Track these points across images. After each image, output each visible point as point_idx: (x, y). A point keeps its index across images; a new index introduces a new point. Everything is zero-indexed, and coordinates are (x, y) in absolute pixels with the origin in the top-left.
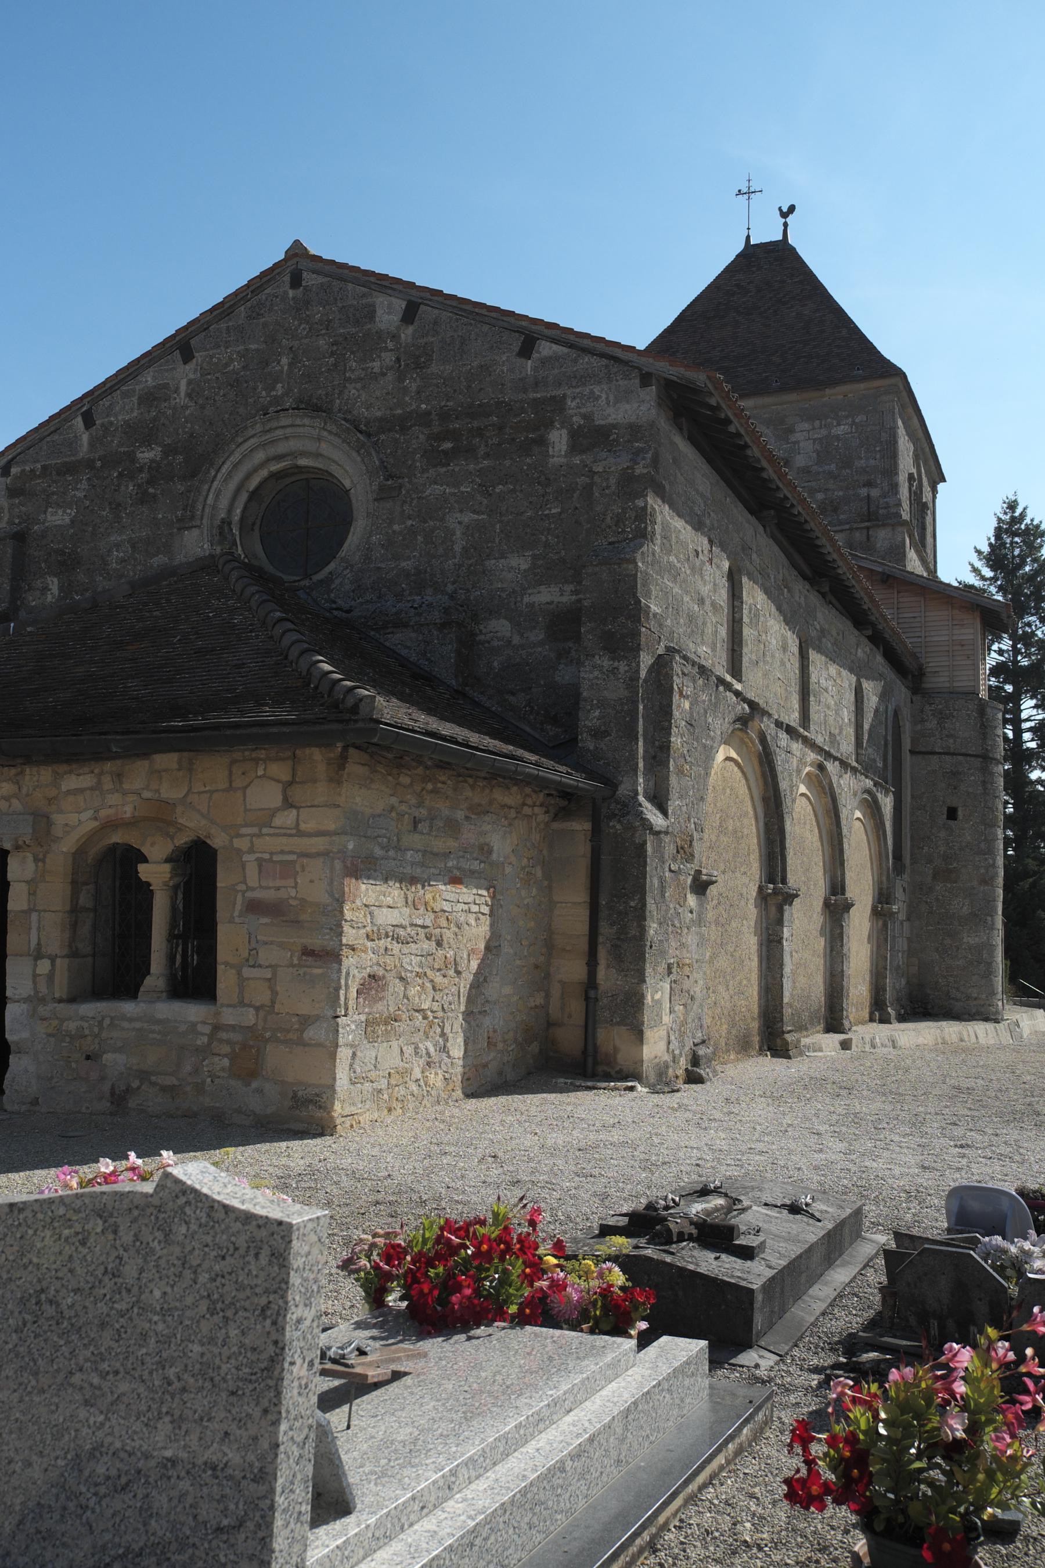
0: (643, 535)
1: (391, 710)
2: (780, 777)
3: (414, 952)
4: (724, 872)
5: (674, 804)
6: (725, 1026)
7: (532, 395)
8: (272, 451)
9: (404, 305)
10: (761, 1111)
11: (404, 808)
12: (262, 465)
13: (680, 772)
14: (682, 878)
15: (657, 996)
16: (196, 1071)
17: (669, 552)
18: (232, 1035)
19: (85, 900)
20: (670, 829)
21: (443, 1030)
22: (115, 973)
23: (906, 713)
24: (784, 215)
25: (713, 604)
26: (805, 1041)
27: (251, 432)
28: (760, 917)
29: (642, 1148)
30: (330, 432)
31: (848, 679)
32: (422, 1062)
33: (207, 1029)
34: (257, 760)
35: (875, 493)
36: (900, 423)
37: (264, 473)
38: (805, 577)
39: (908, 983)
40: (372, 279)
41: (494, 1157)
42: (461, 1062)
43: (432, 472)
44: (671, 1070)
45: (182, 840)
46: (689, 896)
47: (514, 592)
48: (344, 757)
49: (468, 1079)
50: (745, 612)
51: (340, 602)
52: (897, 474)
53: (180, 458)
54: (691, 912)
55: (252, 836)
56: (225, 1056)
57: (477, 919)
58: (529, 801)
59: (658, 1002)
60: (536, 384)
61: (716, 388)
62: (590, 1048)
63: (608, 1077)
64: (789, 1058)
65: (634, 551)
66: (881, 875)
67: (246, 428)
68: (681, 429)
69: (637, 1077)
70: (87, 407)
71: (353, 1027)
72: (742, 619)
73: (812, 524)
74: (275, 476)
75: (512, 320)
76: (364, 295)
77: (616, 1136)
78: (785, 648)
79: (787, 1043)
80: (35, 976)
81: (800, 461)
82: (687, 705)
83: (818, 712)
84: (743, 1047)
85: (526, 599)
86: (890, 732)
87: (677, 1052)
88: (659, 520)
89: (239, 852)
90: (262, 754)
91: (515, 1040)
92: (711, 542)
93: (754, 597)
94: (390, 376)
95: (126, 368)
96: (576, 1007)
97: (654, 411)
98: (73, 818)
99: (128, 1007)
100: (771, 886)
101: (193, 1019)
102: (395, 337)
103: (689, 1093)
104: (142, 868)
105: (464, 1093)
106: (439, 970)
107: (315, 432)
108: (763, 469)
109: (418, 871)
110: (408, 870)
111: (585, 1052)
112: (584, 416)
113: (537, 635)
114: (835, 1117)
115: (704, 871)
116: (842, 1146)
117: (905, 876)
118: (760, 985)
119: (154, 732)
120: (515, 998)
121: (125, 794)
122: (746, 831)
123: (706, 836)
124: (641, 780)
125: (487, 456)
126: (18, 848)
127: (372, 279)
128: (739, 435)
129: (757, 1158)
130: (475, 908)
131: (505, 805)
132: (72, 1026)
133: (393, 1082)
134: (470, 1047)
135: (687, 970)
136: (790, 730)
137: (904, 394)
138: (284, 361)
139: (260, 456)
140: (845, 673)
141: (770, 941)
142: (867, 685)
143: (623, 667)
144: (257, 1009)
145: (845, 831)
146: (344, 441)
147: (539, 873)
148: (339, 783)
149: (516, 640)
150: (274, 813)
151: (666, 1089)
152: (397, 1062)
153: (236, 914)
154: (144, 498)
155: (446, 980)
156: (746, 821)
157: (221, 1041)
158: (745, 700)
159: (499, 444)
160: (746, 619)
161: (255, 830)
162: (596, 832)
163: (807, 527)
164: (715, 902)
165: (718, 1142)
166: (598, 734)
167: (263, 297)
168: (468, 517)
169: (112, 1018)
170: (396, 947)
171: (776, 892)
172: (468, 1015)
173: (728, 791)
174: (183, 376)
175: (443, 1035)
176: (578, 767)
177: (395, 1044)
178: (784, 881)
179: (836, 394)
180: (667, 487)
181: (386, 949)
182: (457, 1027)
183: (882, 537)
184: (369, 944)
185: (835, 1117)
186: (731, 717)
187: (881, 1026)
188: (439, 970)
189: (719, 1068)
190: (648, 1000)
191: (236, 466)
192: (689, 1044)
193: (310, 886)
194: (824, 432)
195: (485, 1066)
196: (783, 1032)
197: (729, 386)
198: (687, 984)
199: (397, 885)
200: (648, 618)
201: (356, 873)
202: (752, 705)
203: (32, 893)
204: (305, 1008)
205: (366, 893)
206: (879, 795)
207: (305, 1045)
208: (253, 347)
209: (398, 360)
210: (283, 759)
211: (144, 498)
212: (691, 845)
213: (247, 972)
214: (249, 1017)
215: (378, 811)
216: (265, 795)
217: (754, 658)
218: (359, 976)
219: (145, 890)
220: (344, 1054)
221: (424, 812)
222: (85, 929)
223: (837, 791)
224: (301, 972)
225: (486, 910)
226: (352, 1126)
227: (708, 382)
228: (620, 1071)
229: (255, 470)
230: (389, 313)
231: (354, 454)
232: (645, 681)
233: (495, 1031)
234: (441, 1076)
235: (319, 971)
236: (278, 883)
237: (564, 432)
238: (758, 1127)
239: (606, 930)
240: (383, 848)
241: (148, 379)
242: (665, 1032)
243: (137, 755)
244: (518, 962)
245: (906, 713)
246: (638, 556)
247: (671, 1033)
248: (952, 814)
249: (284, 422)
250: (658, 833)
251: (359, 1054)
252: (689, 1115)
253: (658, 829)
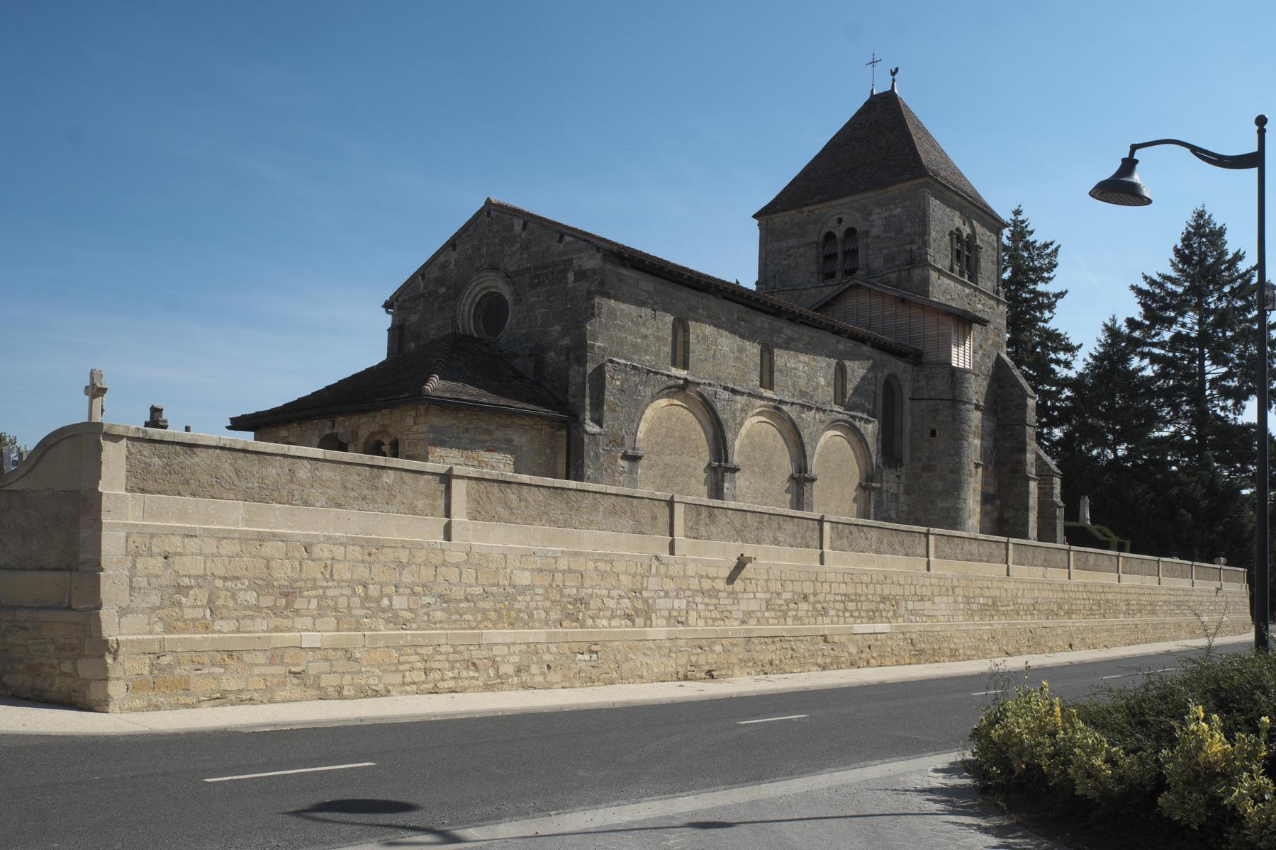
24: (893, 74)
35: (915, 247)
70: (422, 272)
81: (875, 232)
139: (478, 289)
162: (568, 434)
166: (574, 397)
168: (542, 310)
174: (453, 256)
178: (726, 461)
179: (894, 190)
241: (442, 259)
248: (933, 433)
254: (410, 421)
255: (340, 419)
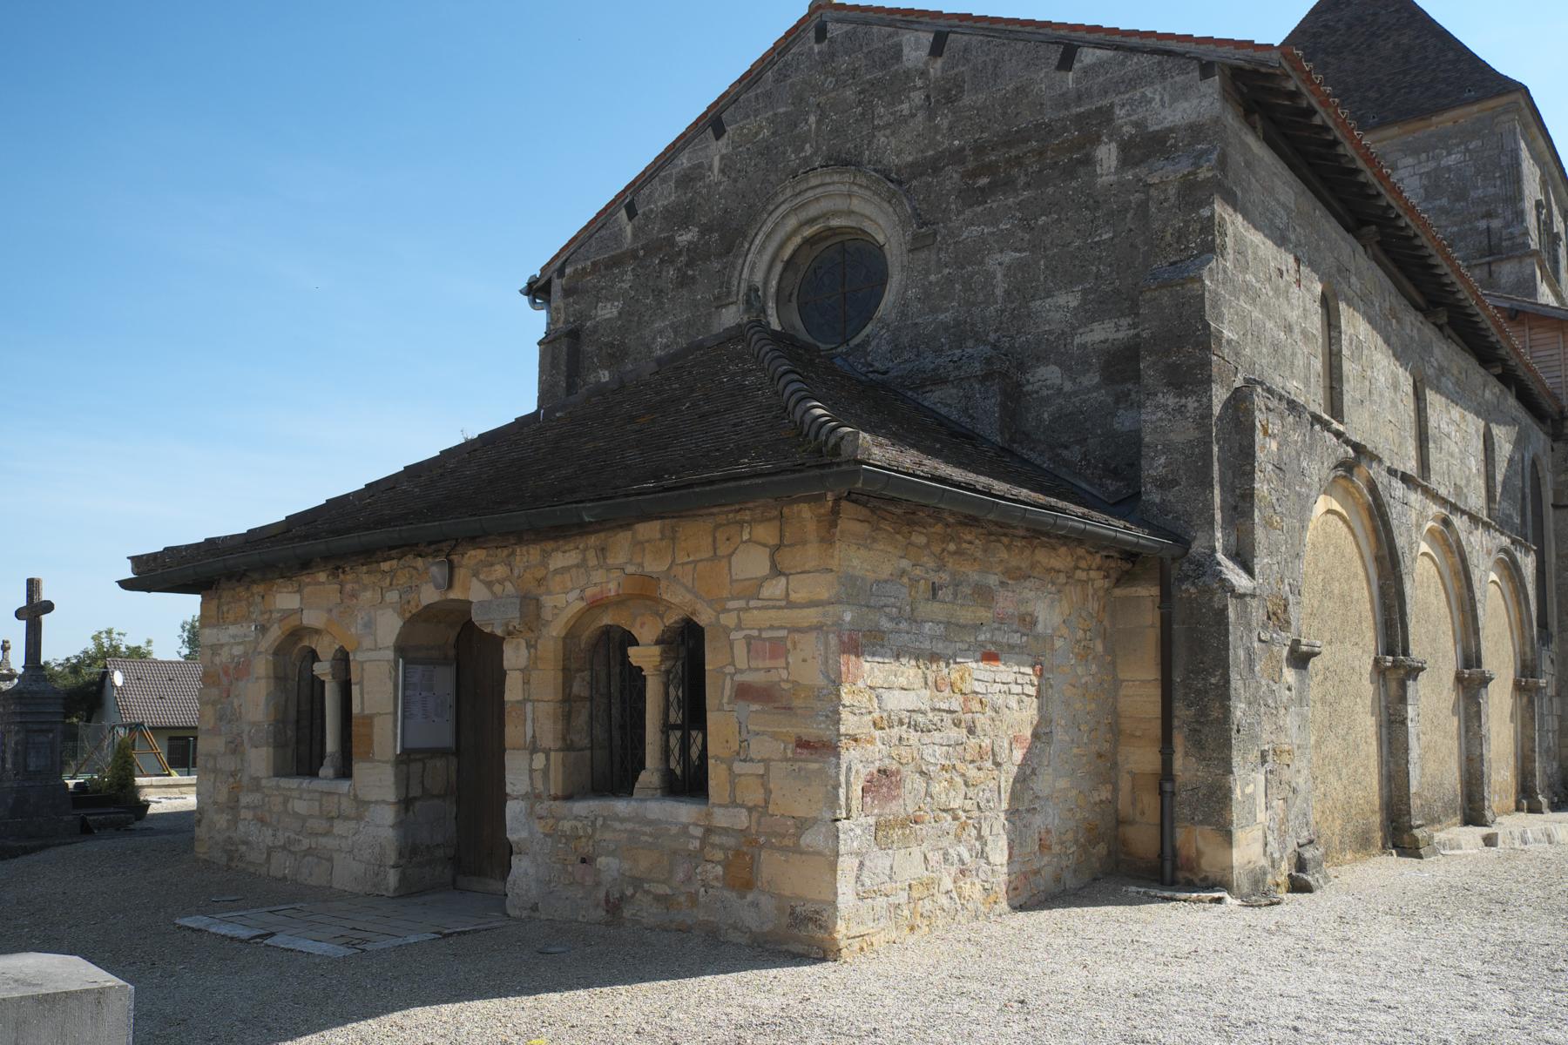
0: (1210, 249)
1: (877, 451)
2: (1396, 532)
3: (937, 741)
4: (1330, 643)
5: (1261, 562)
6: (1338, 822)
7: (1076, 110)
8: (804, 215)
9: (931, 37)
10: (1385, 936)
11: (918, 571)
12: (795, 232)
13: (1268, 524)
14: (1276, 649)
15: (1249, 790)
16: (689, 879)
17: (1245, 269)
18: (724, 840)
19: (579, 688)
20: (1258, 592)
21: (979, 831)
22: (612, 772)
23: (1546, 462)
25: (1304, 333)
26: (1440, 836)
27: (781, 198)
28: (1377, 698)
29: (1219, 997)
30: (861, 186)
31: (1475, 425)
32: (954, 870)
33: (698, 832)
34: (741, 523)
35: (1496, 224)
36: (1523, 145)
37: (798, 240)
38: (1417, 308)
39: (1560, 766)
40: (898, 17)
41: (1022, 1002)
42: (1005, 869)
43: (968, 213)
44: (1269, 877)
45: (672, 619)
46: (1285, 670)
47: (1063, 333)
48: (835, 512)
49: (1015, 889)
50: (1345, 343)
51: (877, 364)
52: (1522, 200)
53: (716, 235)
54: (1289, 689)
55: (739, 610)
56: (719, 863)
57: (1020, 702)
58: (1083, 564)
59: (1252, 797)
60: (1079, 98)
61: (1294, 69)
62: (1168, 850)
63: (1191, 886)
64: (1420, 857)
65: (1203, 265)
66: (1523, 645)
67: (776, 194)
68: (1253, 128)
69: (1226, 885)
70: (628, 201)
71: (859, 831)
72: (1340, 351)
73: (1424, 239)
74: (809, 242)
75: (1049, 31)
76: (890, 36)
77: (1188, 974)
78: (1395, 386)
79: (1417, 840)
80: (531, 771)
82: (1274, 446)
83: (1440, 460)
84: (1363, 844)
85: (1077, 340)
86: (1528, 484)
87: (1276, 855)
88: (1230, 231)
89: (726, 630)
90: (747, 515)
91: (1076, 842)
92: (1297, 260)
93: (1354, 326)
94: (920, 116)
95: (663, 154)
96: (1150, 802)
97: (1218, 105)
98: (560, 600)
99: (621, 806)
100: (1390, 658)
101: (684, 819)
102: (923, 74)
103: (1294, 903)
104: (632, 651)
105: (1010, 905)
106: (972, 762)
107: (845, 189)
108: (1358, 171)
109: (939, 647)
110: (927, 645)
111: (1161, 855)
112: (1136, 125)
113: (1092, 379)
114: (1488, 948)
115: (1304, 641)
116: (1504, 1000)
117: (1553, 646)
118: (1380, 774)
119: (627, 496)
120: (1074, 792)
121: (608, 570)
122: (1355, 595)
123: (1305, 600)
124: (1219, 535)
125: (1028, 185)
126: (510, 634)
127: (898, 17)
128: (1325, 128)
129: (1382, 1017)
130: (1016, 689)
131: (1052, 569)
132: (566, 825)
133: (915, 894)
134: (1016, 851)
135: (1286, 758)
136: (1405, 478)
137: (1527, 112)
138: (812, 119)
139: (792, 222)
140: (1470, 417)
141: (1391, 722)
142: (1498, 431)
143: (1191, 403)
144: (750, 810)
145: (1478, 595)
146: (875, 193)
147: (1099, 647)
148: (831, 543)
149: (1068, 386)
150: (760, 582)
151: (1264, 901)
152: (919, 870)
153: (725, 700)
154: (684, 281)
155: (981, 774)
156: (1355, 584)
157: (713, 846)
158: (1348, 442)
159: (1041, 171)
160: (1345, 351)
161: (742, 604)
162: (1166, 596)
163: (1417, 242)
164: (1320, 677)
165: (1326, 987)
166: (1164, 484)
167: (789, 57)
168: (1009, 257)
169: (605, 818)
170: (914, 736)
171: (1396, 665)
172: (1012, 813)
173: (1332, 549)
174: (716, 151)
175: (980, 837)
176: (1142, 523)
177: (915, 850)
178: (1406, 652)
179: (1444, 121)
180: (1239, 194)
181: (900, 739)
182: (998, 828)
183: (1507, 272)
184: (877, 733)
185: (1488, 948)
186: (1332, 461)
187: (1531, 816)
188: (972, 762)
189: (1332, 872)
190: (1237, 794)
191: (768, 236)
192: (1292, 845)
193: (804, 664)
194: (1432, 165)
195: (1037, 872)
196: (1411, 828)
197: (1311, 65)
198: (1287, 774)
199: (913, 662)
200: (1220, 345)
201: (855, 648)
202: (1357, 447)
203: (526, 682)
204: (801, 810)
205: (870, 670)
206: (1518, 555)
207: (802, 853)
208: (782, 110)
209: (928, 97)
210: (769, 520)
211: (684, 281)
212: (1285, 610)
213: (738, 767)
214: (742, 820)
215: (884, 576)
216: (751, 563)
217: (1358, 396)
218: (864, 772)
219: (635, 677)
220: (847, 865)
221: (945, 577)
222: (581, 719)
223: (1467, 549)
224: (796, 767)
225: (1032, 691)
226: (862, 949)
227: (1285, 64)
228: (1206, 878)
229: (789, 238)
230: (917, 49)
231: (886, 205)
232: (1220, 418)
233: (1048, 832)
234: (978, 887)
235: (814, 766)
236: (768, 664)
237: (1113, 146)
238: (1383, 964)
239: (1182, 712)
240: (892, 619)
241: (684, 161)
242: (1261, 833)
243: (621, 527)
244: (1075, 751)
245: (1546, 462)
246: (1205, 273)
247: (1269, 833)
249: (813, 182)
250: (1242, 596)
251: (867, 863)
252: (1289, 941)
253: (1242, 591)
254: (751, 563)
255: (475, 556)
